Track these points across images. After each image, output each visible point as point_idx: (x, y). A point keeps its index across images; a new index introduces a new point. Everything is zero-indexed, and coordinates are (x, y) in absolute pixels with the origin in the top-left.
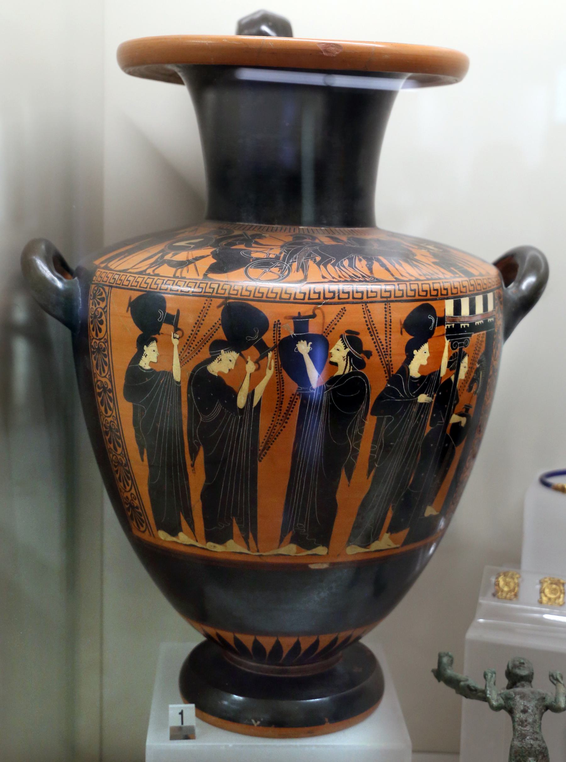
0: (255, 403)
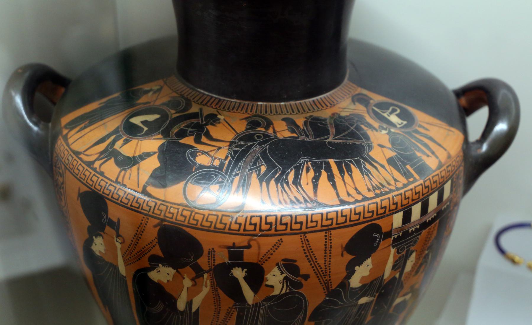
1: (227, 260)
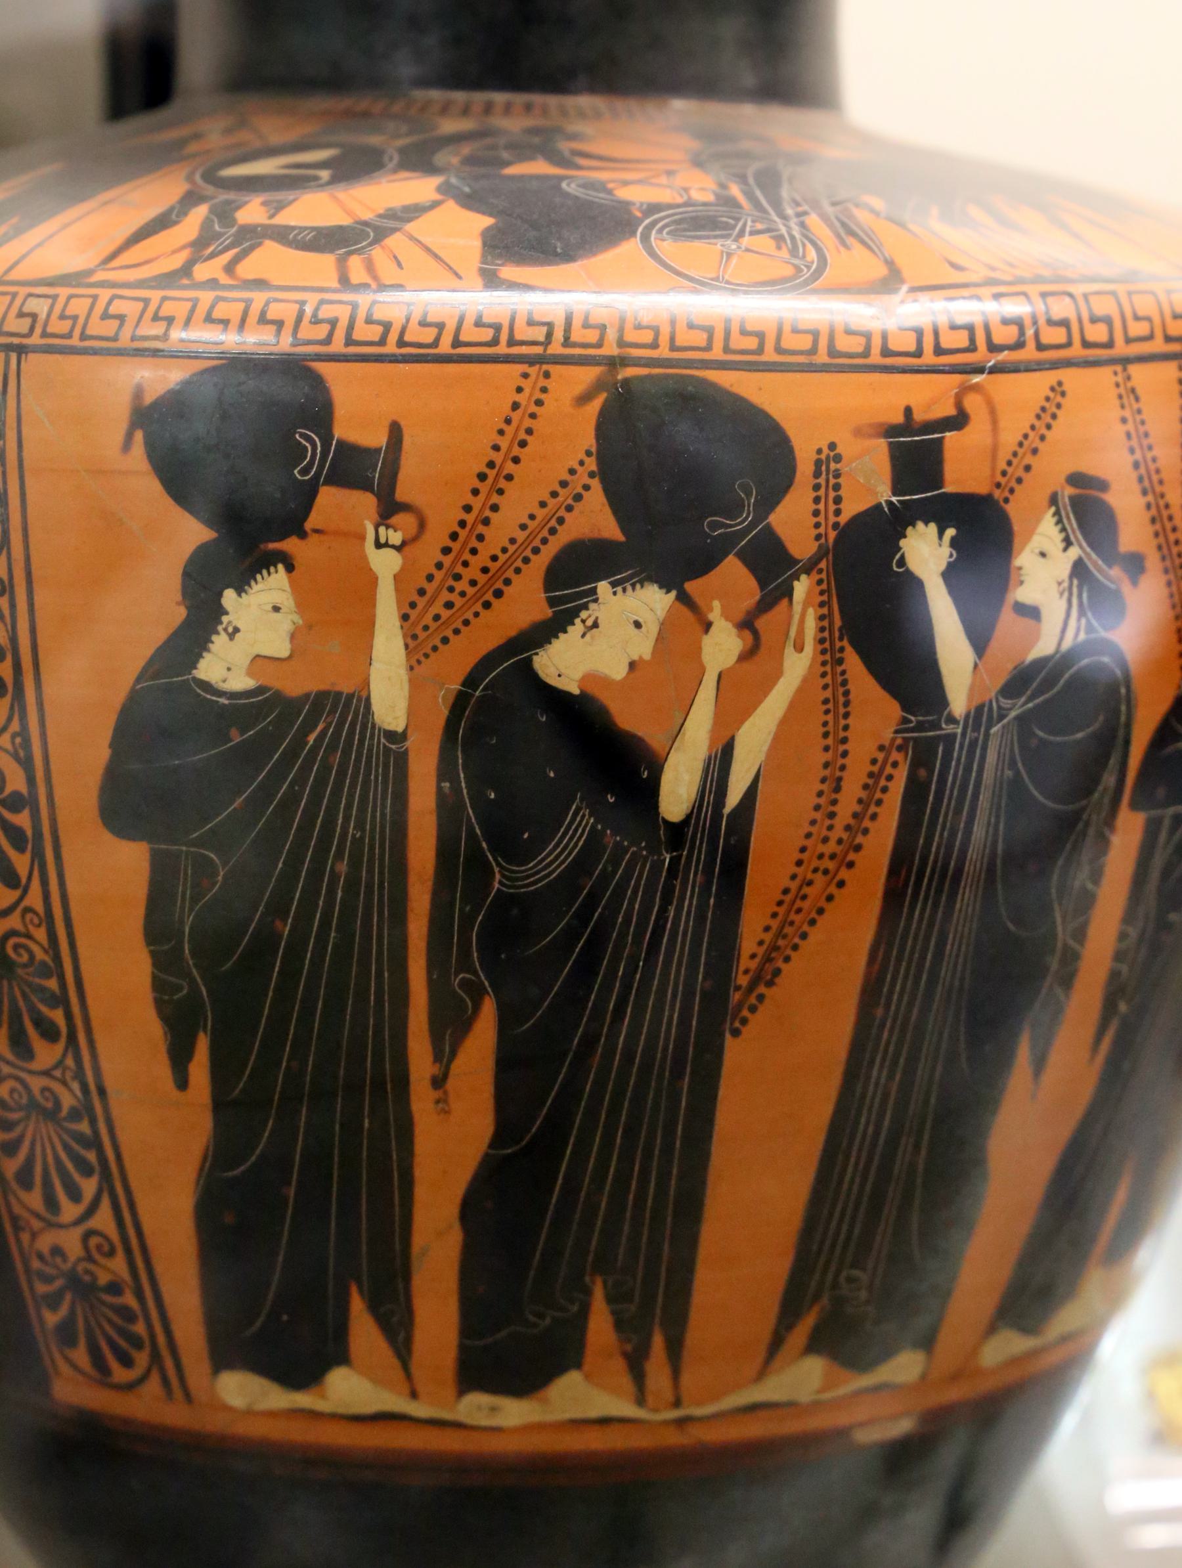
0: (733, 798)
1: (884, 494)
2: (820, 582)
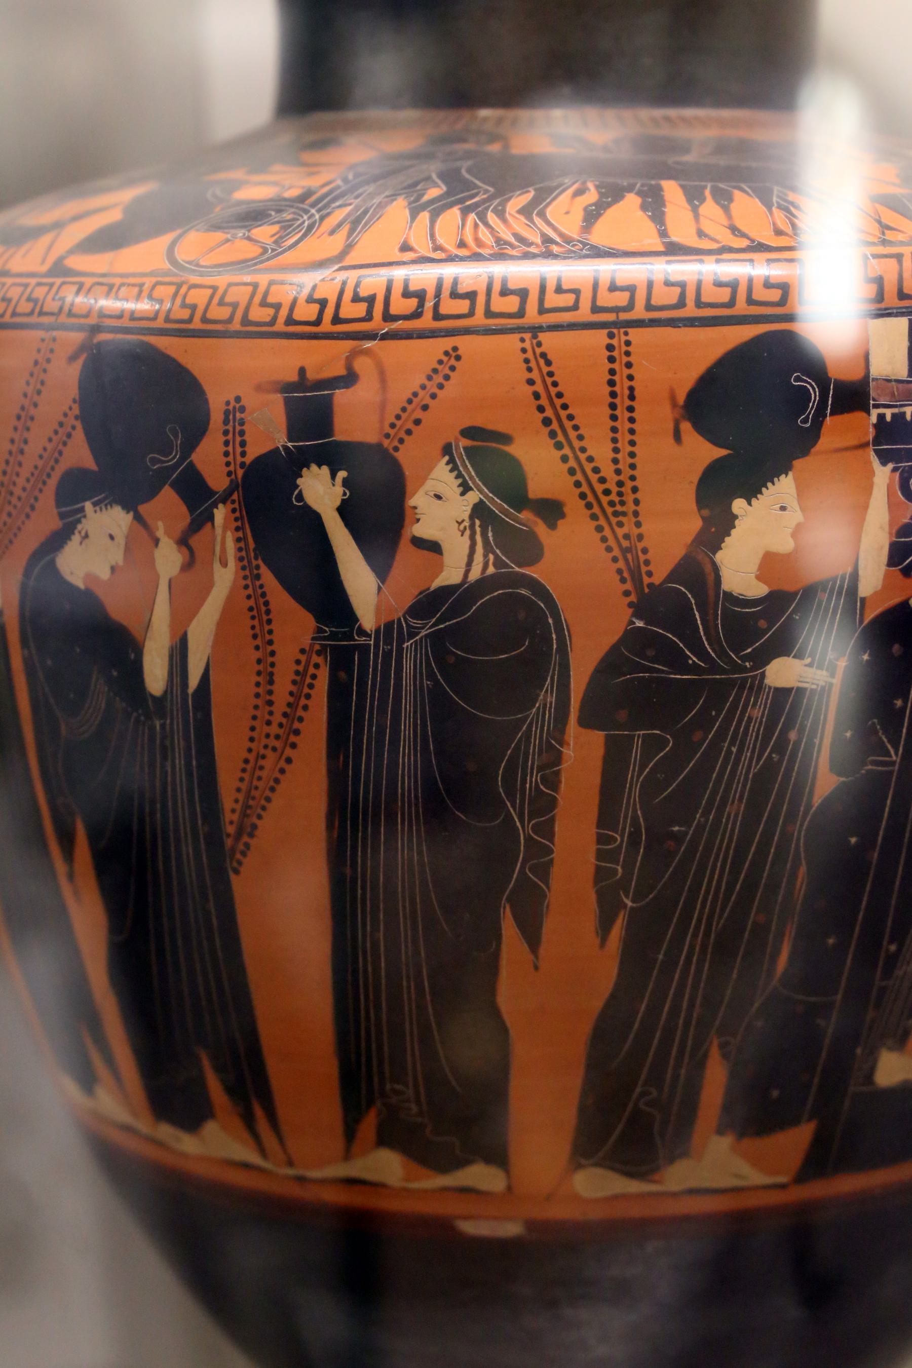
0: (194, 681)
1: (281, 440)
2: (234, 511)
